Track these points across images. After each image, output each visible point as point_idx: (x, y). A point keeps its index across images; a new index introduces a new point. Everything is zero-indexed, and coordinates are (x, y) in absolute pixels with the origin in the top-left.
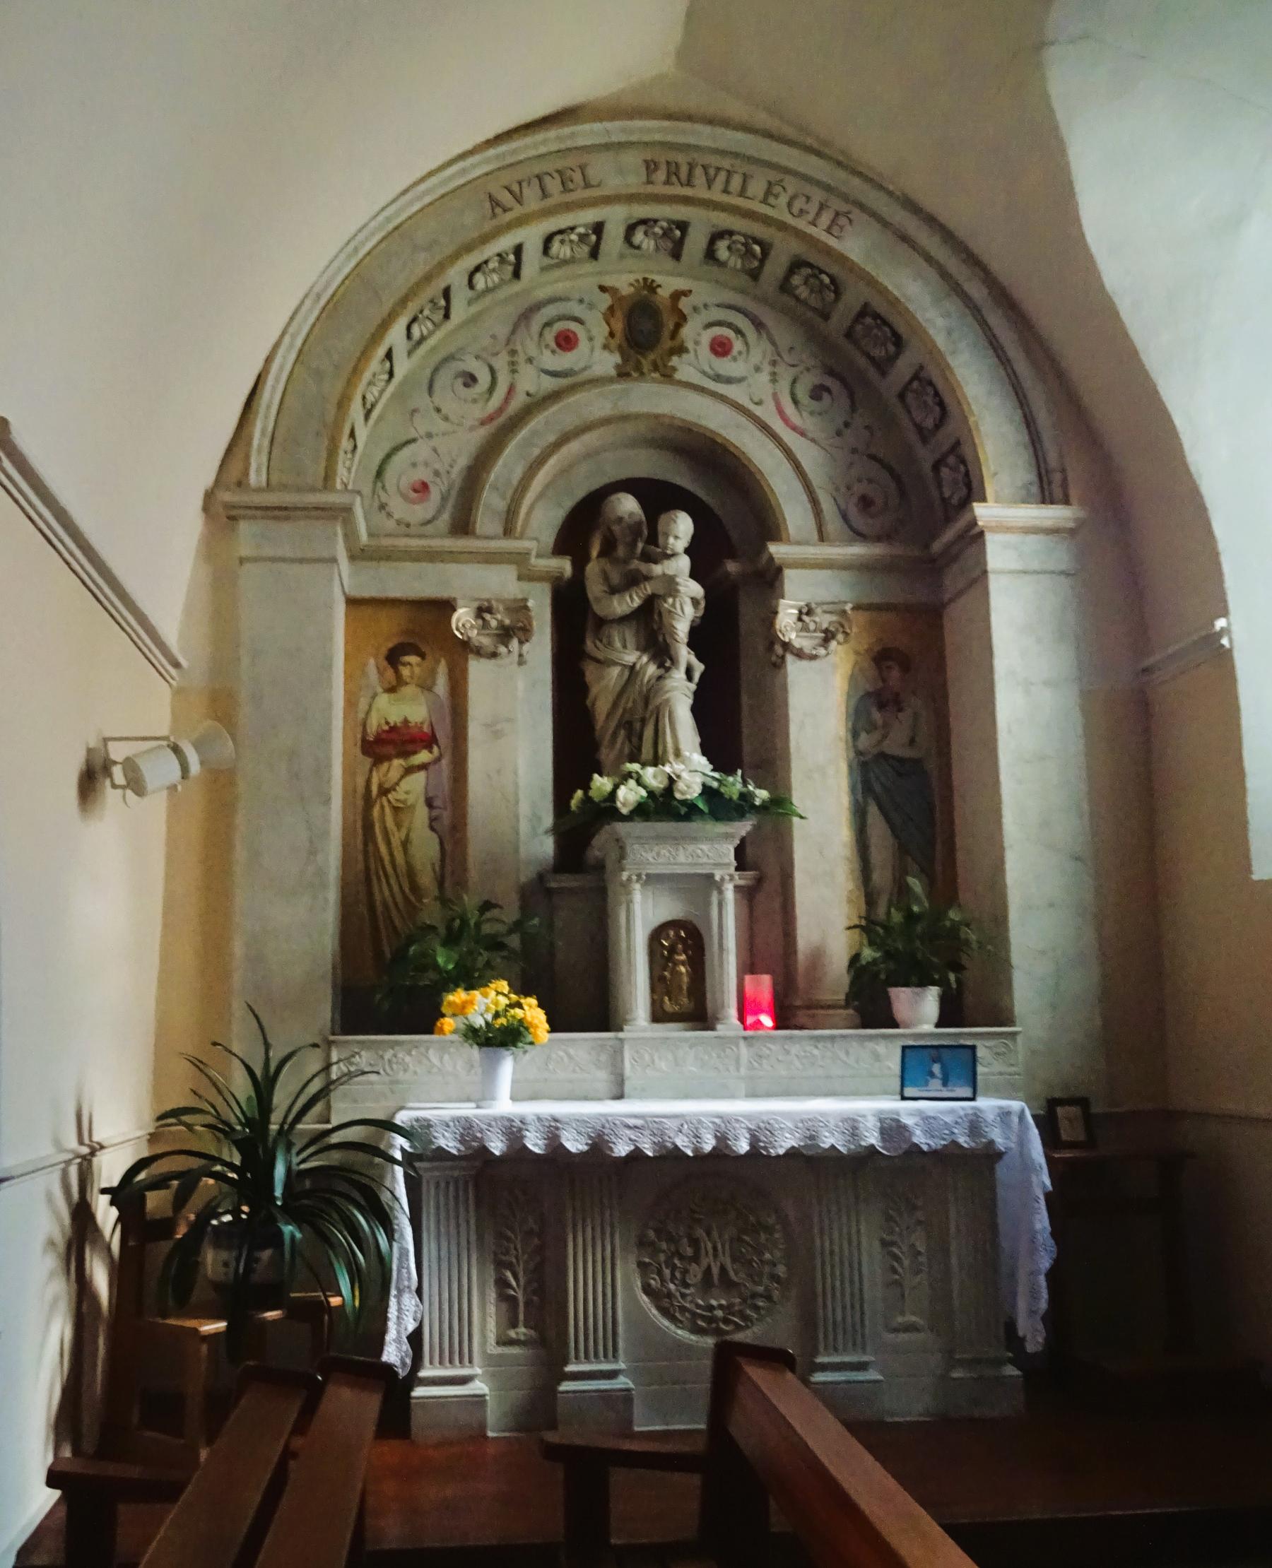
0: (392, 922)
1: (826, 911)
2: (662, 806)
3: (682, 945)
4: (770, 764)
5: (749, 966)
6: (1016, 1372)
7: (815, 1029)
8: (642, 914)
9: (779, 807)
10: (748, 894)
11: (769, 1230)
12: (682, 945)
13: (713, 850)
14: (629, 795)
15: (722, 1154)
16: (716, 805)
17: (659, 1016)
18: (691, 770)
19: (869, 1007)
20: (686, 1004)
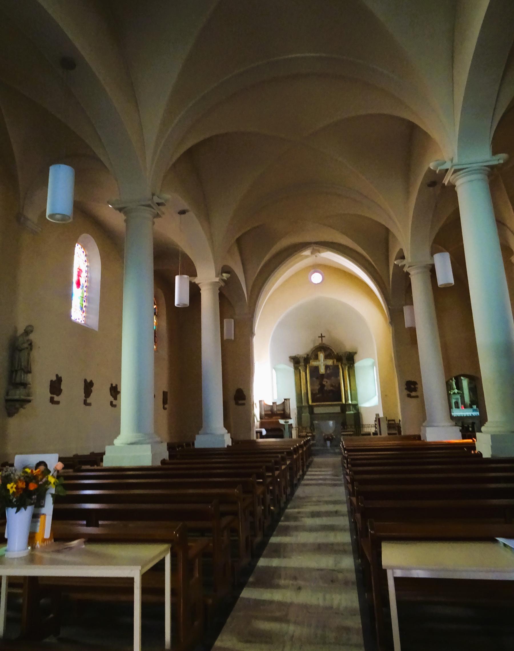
0: (246, 278)
1: (467, 399)
2: (454, 393)
3: (456, 403)
4: (462, 390)
5: (462, 404)
6: (79, 250)
7: (495, 131)
8: (453, 401)
9: (463, 393)
10: (461, 399)
11: (345, 449)
12: (456, 403)
13: (458, 396)
14: (452, 393)
15: (461, 417)
16: (458, 393)
17: (455, 408)
18: (456, 391)
19: (471, 406)
20: (457, 407)
